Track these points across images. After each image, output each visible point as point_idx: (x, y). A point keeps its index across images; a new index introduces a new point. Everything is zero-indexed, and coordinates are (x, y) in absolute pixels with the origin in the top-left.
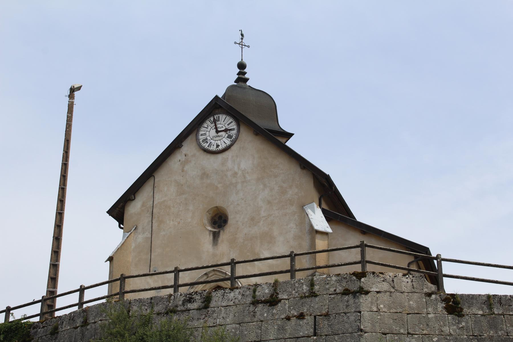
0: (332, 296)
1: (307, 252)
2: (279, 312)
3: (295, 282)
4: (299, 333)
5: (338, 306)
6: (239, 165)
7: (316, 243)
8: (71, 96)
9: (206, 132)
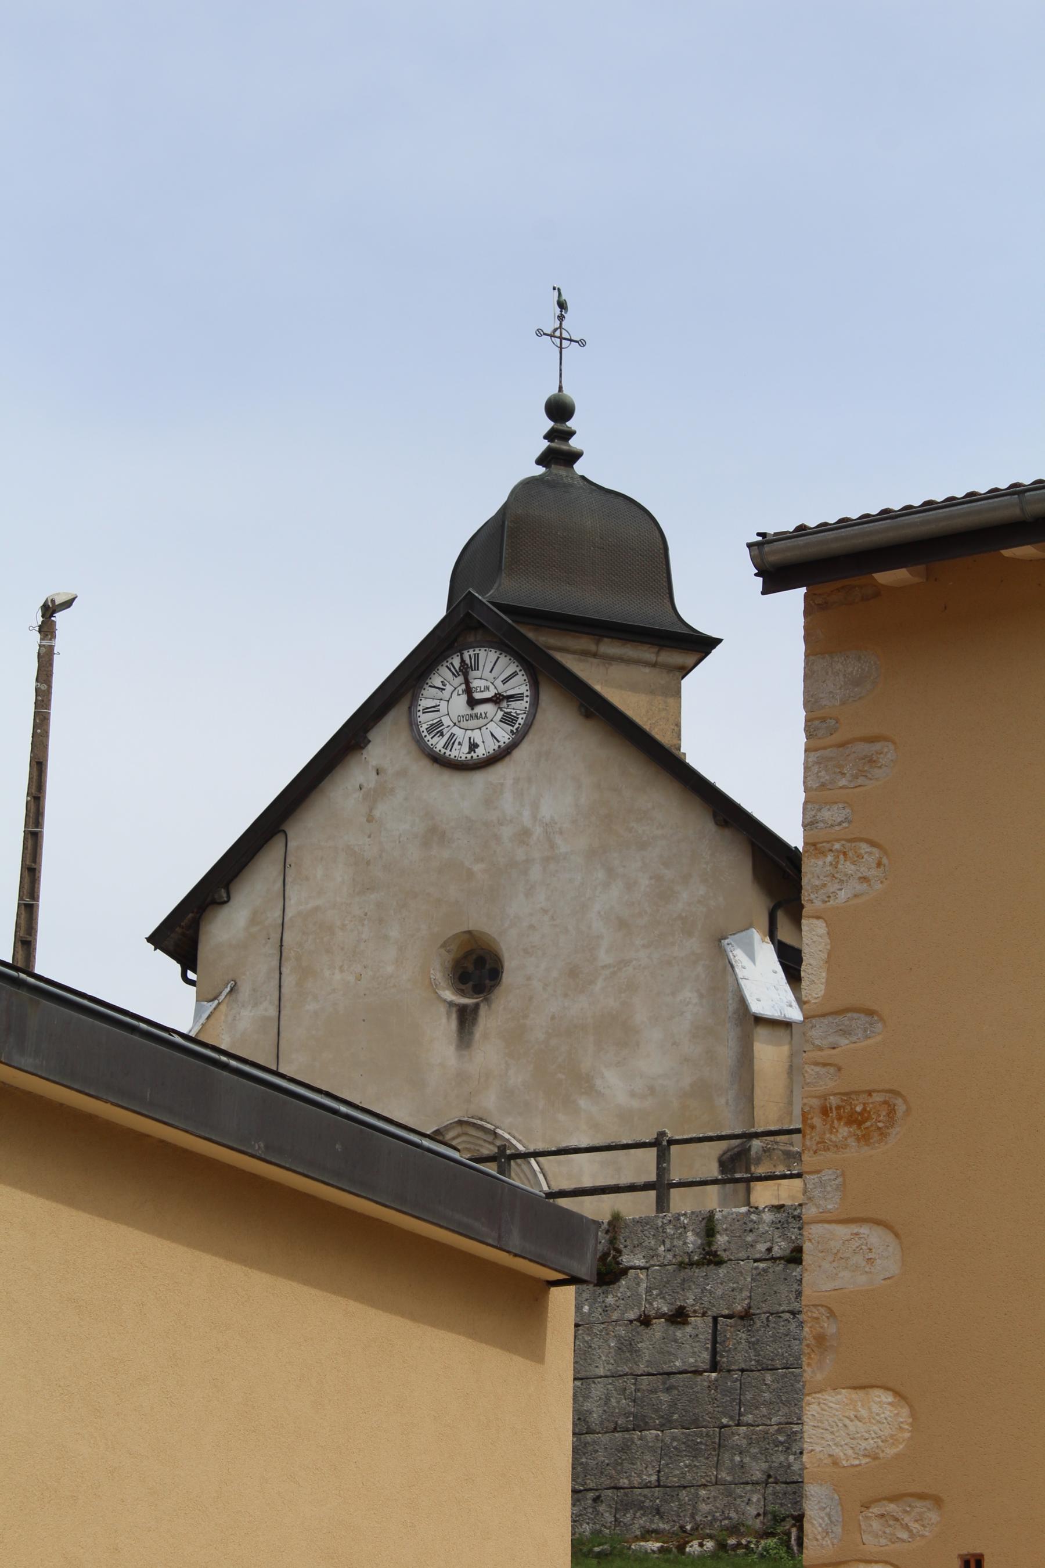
0: (762, 1265)
1: (701, 1135)
2: (622, 1302)
3: (665, 1222)
4: (673, 1362)
5: (776, 1292)
6: (535, 806)
7: (756, 1054)
8: (47, 629)
9: (437, 702)
